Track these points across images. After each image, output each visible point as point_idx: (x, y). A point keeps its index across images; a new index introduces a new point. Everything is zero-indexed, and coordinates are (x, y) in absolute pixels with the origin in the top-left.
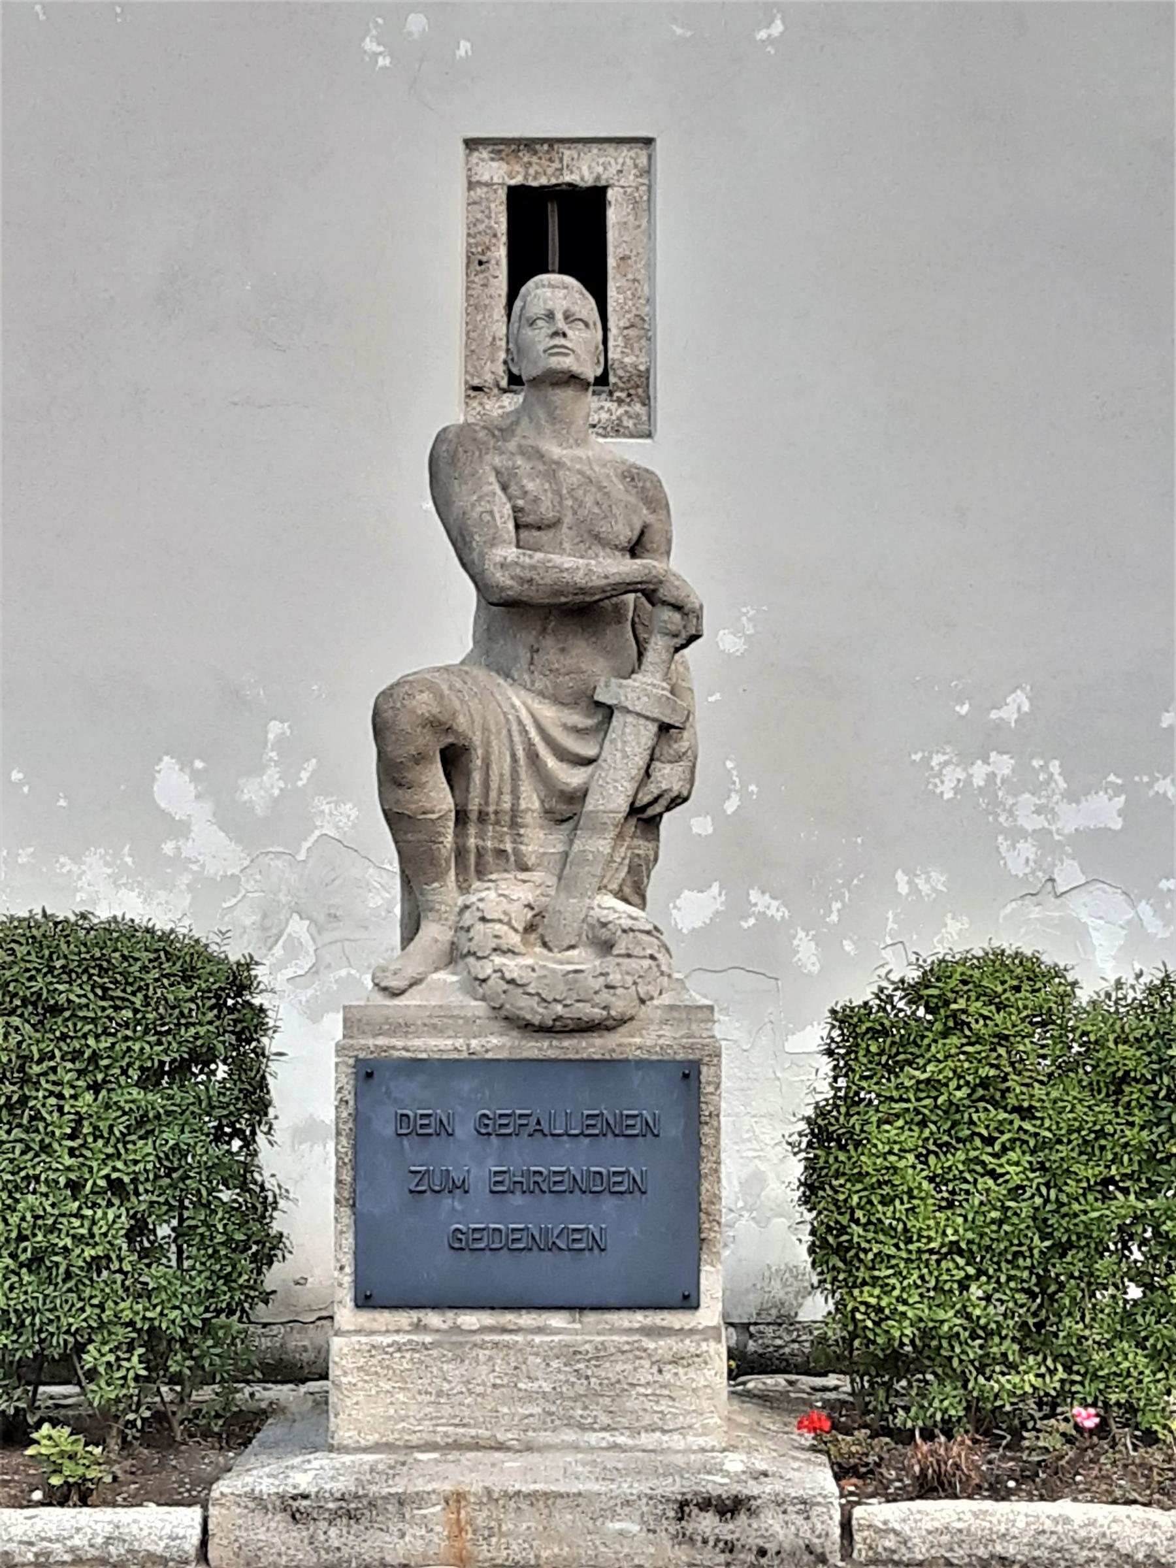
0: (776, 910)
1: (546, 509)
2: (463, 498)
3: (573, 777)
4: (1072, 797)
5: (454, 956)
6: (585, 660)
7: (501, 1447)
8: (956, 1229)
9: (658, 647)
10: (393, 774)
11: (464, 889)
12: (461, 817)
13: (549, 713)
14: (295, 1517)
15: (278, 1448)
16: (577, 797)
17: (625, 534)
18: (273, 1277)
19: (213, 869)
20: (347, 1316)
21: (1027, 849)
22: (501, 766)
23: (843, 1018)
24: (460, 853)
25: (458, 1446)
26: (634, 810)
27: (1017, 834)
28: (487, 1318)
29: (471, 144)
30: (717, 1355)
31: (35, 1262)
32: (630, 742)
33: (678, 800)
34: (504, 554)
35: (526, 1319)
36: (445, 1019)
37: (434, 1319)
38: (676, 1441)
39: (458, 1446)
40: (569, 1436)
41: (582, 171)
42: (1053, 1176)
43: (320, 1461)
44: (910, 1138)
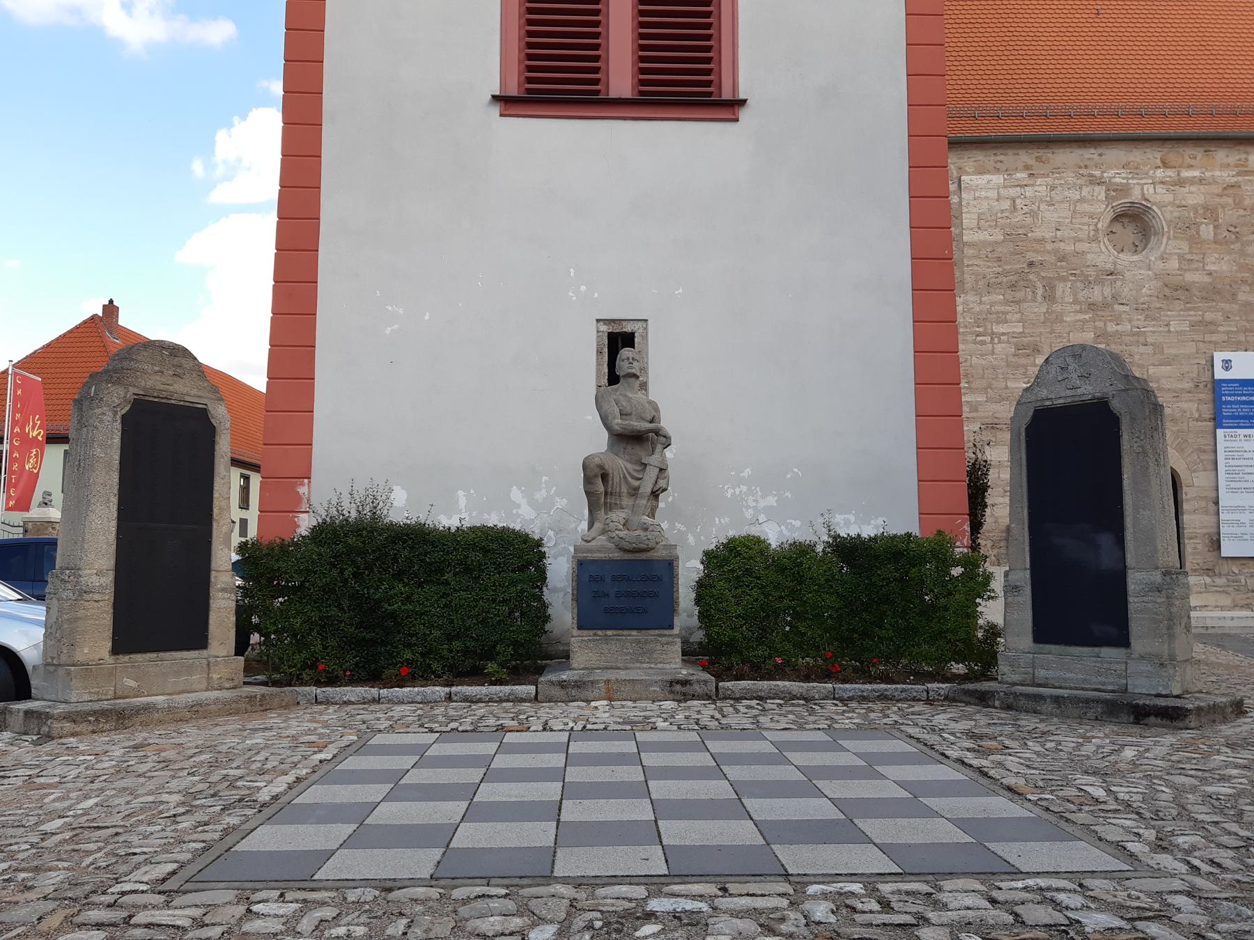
0: (683, 528)
1: (628, 410)
2: (605, 407)
3: (636, 483)
4: (763, 497)
5: (604, 532)
6: (639, 451)
7: (619, 668)
8: (740, 610)
9: (659, 447)
10: (588, 480)
11: (606, 513)
12: (606, 493)
13: (629, 466)
14: (562, 687)
15: (552, 672)
16: (637, 489)
17: (650, 418)
18: (547, 627)
19: (527, 517)
20: (575, 632)
21: (751, 511)
22: (617, 480)
23: (706, 553)
24: (605, 503)
25: (606, 668)
26: (653, 492)
27: (748, 507)
28: (614, 632)
29: (598, 321)
30: (678, 648)
31: (482, 622)
32: (652, 473)
33: (665, 490)
34: (617, 422)
35: (625, 632)
36: (603, 548)
37: (600, 632)
38: (668, 666)
39: (606, 668)
40: (638, 665)
41: (628, 328)
42: (766, 595)
43: (568, 672)
44: (727, 585)
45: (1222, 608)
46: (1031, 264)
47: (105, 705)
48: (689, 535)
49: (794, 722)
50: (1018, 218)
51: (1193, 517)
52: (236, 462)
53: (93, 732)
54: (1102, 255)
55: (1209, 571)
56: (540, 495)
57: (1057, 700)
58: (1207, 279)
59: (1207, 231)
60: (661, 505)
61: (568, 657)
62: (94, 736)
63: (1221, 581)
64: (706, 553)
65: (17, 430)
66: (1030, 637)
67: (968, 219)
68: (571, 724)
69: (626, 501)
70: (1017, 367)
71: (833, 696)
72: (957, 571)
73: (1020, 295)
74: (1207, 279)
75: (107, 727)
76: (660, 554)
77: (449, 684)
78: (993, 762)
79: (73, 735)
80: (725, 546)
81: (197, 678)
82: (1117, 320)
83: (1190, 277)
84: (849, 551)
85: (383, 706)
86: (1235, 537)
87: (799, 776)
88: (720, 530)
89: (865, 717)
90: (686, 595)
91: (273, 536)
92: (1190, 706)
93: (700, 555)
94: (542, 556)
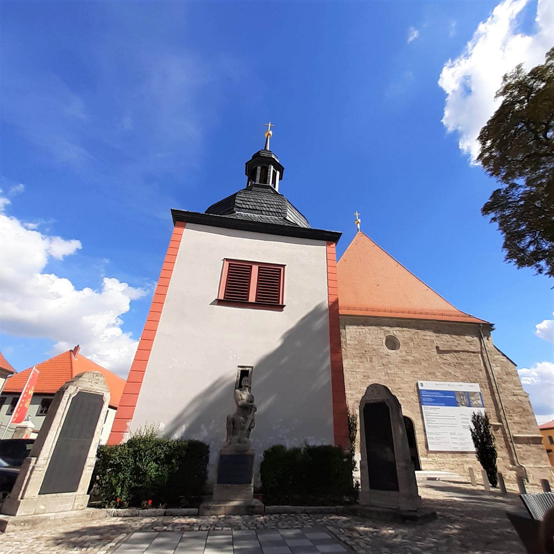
3: (244, 425)
10: (228, 423)
16: (244, 427)
20: (216, 485)
37: (225, 485)
45: (432, 470)
46: (365, 351)
47: (29, 517)
48: (258, 444)
49: (290, 525)
50: (361, 338)
51: (419, 436)
52: (110, 407)
53: (21, 530)
54: (386, 350)
55: (426, 456)
56: (211, 427)
57: (378, 513)
58: (413, 358)
59: (411, 344)
60: (252, 431)
61: (212, 494)
62: (21, 532)
63: (430, 459)
64: (265, 452)
65: (23, 401)
66: (368, 486)
67: (348, 337)
68: (209, 527)
69: (240, 432)
70: (363, 382)
71: (304, 512)
72: (345, 460)
73: (363, 360)
74: (413, 358)
75: (28, 528)
76: (249, 452)
77: (166, 508)
78: (356, 542)
79: (13, 531)
80: (272, 449)
81: (69, 506)
82: (390, 369)
83: (408, 357)
84: (312, 451)
85: (139, 518)
86: (434, 443)
87: (307, 535)
88: (270, 442)
89: (315, 522)
90: (256, 469)
91: (113, 443)
92: (419, 516)
93: (263, 452)
94: (208, 452)
